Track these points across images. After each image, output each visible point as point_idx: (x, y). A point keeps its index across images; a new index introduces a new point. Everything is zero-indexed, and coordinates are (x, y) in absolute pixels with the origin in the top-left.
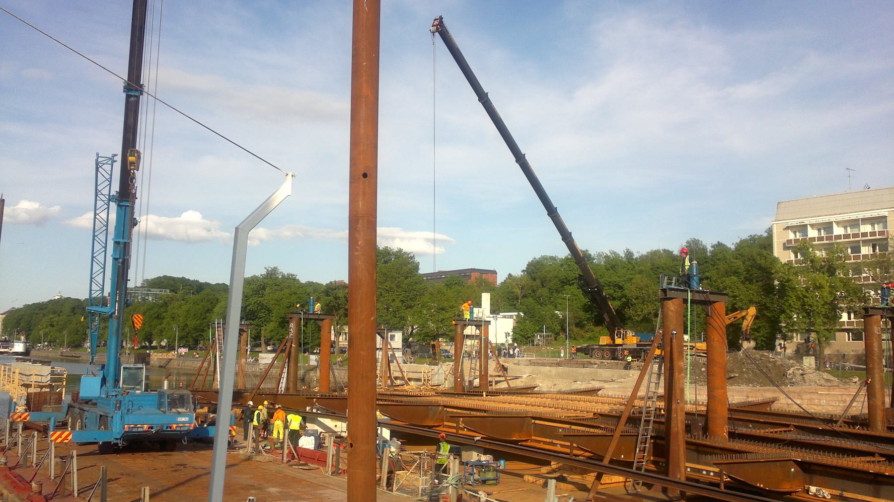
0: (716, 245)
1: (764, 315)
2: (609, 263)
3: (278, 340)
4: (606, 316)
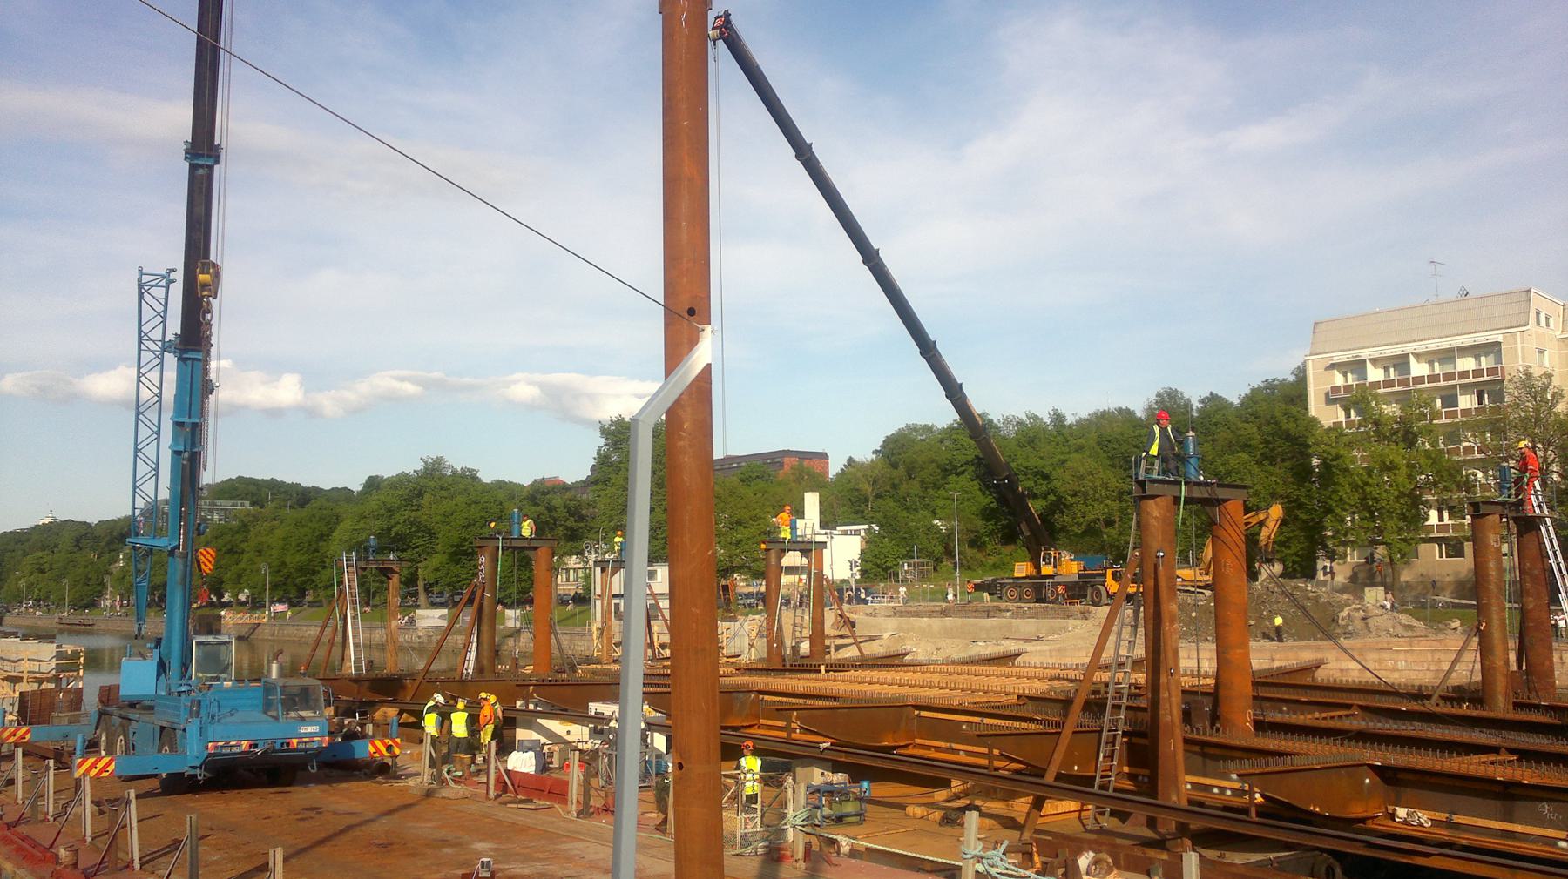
0: (1207, 398)
1: (1296, 518)
2: (1024, 433)
3: (449, 585)
4: (1024, 526)
